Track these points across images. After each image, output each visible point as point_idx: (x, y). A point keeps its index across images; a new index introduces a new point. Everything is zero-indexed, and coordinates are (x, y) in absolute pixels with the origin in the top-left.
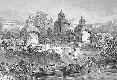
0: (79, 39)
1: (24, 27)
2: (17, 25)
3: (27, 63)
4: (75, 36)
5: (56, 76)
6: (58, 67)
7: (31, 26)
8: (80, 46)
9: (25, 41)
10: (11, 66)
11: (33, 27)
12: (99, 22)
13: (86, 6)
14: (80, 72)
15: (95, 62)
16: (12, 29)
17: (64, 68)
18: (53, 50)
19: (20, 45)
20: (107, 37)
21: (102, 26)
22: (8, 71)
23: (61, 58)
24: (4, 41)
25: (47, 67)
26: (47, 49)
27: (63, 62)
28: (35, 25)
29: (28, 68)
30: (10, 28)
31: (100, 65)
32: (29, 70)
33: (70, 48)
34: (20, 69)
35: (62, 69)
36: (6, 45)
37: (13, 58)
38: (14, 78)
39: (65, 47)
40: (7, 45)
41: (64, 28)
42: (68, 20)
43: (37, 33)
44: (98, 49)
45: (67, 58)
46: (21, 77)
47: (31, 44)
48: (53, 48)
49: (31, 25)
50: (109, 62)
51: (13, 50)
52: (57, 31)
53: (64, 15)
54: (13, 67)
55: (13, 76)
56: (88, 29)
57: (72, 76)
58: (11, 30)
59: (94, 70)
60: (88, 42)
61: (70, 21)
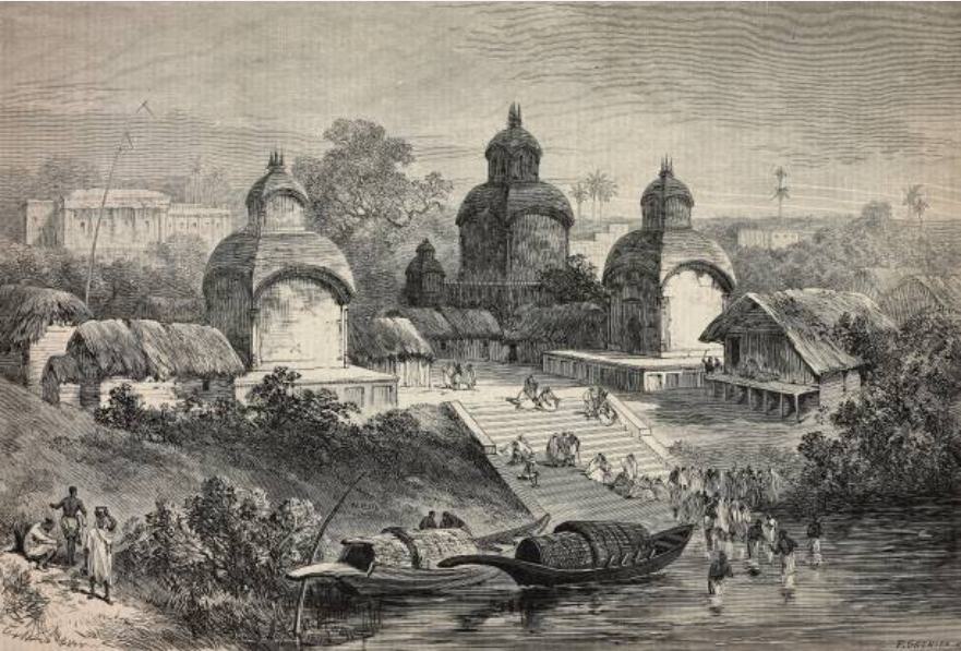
0: (644, 336)
1: (234, 236)
3: (254, 508)
4: (616, 310)
5: (465, 609)
6: (484, 543)
8: (650, 383)
9: (242, 346)
10: (127, 527)
12: (792, 208)
13: (702, 85)
14: (647, 581)
15: (762, 506)
17: (529, 549)
18: (449, 413)
20: (853, 316)
21: (818, 238)
22: (102, 562)
23: (509, 475)
24: (78, 339)
26: (406, 400)
27: (519, 506)
29: (260, 544)
31: (798, 532)
32: (264, 560)
33: (574, 396)
34: (195, 550)
35: (509, 552)
36: (93, 371)
37: (147, 470)
38: (149, 618)
39: (539, 392)
40: (104, 365)
42: (566, 189)
43: (327, 281)
44: (783, 408)
45: (552, 471)
46: (202, 613)
47: (282, 365)
50: (860, 506)
51: (146, 407)
53: (533, 153)
54: (145, 536)
55: (140, 604)
56: (707, 257)
57: (586, 608)
59: (754, 563)
60: (708, 354)
61: (579, 195)
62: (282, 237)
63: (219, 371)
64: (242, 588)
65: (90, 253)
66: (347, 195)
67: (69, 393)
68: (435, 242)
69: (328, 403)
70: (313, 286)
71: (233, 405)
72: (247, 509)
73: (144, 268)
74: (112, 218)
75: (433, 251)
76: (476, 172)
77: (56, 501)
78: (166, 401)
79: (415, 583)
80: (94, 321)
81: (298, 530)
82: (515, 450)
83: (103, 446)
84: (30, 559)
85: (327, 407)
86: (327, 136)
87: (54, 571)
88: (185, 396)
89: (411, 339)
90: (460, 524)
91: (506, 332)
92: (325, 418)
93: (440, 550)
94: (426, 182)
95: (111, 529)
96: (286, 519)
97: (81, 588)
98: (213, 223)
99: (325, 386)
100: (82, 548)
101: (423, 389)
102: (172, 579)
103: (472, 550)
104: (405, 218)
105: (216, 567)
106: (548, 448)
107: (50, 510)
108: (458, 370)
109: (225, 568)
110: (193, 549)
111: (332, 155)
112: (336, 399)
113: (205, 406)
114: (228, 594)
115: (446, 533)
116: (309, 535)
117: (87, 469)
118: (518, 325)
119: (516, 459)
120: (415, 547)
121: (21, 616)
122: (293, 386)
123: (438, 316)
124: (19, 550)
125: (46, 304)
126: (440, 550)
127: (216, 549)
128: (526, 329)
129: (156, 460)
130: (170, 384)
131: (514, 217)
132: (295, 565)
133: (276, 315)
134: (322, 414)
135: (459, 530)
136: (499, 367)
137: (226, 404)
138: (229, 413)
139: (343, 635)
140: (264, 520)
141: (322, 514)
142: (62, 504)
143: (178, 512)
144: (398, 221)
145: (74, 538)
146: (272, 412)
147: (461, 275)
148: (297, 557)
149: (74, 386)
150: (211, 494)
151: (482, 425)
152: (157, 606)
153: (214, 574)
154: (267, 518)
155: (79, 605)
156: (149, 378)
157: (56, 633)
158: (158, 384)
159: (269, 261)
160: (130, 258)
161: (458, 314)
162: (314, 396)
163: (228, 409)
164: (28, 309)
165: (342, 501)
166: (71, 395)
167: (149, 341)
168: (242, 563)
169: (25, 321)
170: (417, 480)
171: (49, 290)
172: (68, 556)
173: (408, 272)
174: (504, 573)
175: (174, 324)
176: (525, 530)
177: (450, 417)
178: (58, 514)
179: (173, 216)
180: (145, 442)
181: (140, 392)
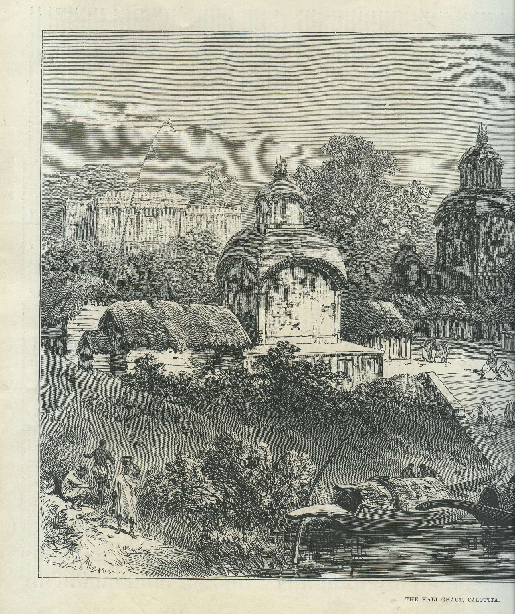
1: (242, 232)
2: (199, 218)
3: (258, 459)
5: (438, 545)
6: (453, 490)
7: (287, 228)
9: (250, 323)
10: (149, 473)
11: (302, 236)
16: (166, 240)
17: (490, 496)
18: (424, 379)
19: (212, 339)
22: (128, 502)
23: (476, 434)
24: (108, 317)
25: (386, 486)
26: (390, 371)
27: (483, 460)
28: (316, 222)
29: (264, 489)
30: (151, 235)
32: (267, 502)
34: (211, 494)
35: (474, 497)
36: (121, 343)
37: (165, 426)
38: (168, 550)
39: (499, 365)
40: (131, 339)
41: (497, 243)
43: (324, 271)
46: (214, 545)
47: (284, 340)
48: (428, 367)
49: (287, 219)
51: (166, 374)
52: (456, 258)
54: (164, 482)
55: (161, 539)
58: (156, 246)
62: (285, 233)
63: (230, 345)
64: (249, 524)
65: (119, 245)
66: (341, 198)
67: (100, 361)
68: (415, 239)
69: (323, 372)
70: (311, 275)
71: (241, 373)
72: (253, 460)
73: (165, 259)
74: (138, 216)
75: (414, 246)
76: (451, 181)
77: (89, 453)
78: (183, 370)
79: (396, 523)
80: (122, 302)
81: (297, 477)
82: (480, 413)
83: (130, 406)
84: (66, 500)
85: (323, 376)
86: (324, 149)
87: (87, 510)
88: (200, 365)
89: (394, 319)
90: (434, 474)
91: (474, 315)
92: (321, 385)
93: (417, 496)
94: (409, 189)
95: (136, 475)
96: (287, 468)
97: (109, 524)
98: (225, 221)
99: (321, 358)
100: (111, 491)
101: (405, 361)
102: (188, 517)
103: (446, 496)
104: (390, 218)
105: (226, 507)
106: (505, 412)
107: (84, 459)
108: (434, 346)
109: (234, 509)
110: (207, 492)
111: (329, 165)
112: (331, 368)
113: (217, 373)
114: (236, 530)
115: (422, 482)
116: (306, 482)
117: (115, 425)
118: (484, 308)
119: (480, 420)
120: (396, 493)
121: (59, 547)
122: (293, 358)
123: (417, 299)
124: (57, 492)
125: (81, 287)
126: (417, 496)
127: (226, 493)
128: (489, 312)
129: (174, 418)
130: (187, 355)
131: (482, 218)
132: (294, 506)
133: (279, 300)
134: (318, 382)
135: (434, 479)
136: (468, 344)
137: (238, 373)
138: (238, 379)
139: (334, 565)
140: (267, 469)
141: (318, 466)
142: (93, 454)
143: (193, 462)
144: (384, 221)
145: (104, 483)
146: (275, 378)
147: (438, 266)
148: (296, 499)
149: (105, 356)
150: (222, 447)
151: (453, 392)
152: (175, 539)
153: (224, 513)
154: (270, 467)
155: (107, 539)
156: (169, 350)
157: (88, 562)
158: (177, 355)
159: (274, 253)
160: (154, 248)
161: (434, 299)
162: (311, 366)
163: (237, 376)
164: (67, 291)
165: (333, 455)
166: (102, 363)
167: (170, 319)
168: (248, 504)
169: (63, 302)
170: (398, 437)
171: (84, 276)
172: (99, 497)
173: (392, 264)
174: (470, 515)
175: (192, 305)
176: (485, 481)
177: (427, 386)
178: (90, 463)
179: (190, 214)
180: (165, 403)
181: (160, 361)
